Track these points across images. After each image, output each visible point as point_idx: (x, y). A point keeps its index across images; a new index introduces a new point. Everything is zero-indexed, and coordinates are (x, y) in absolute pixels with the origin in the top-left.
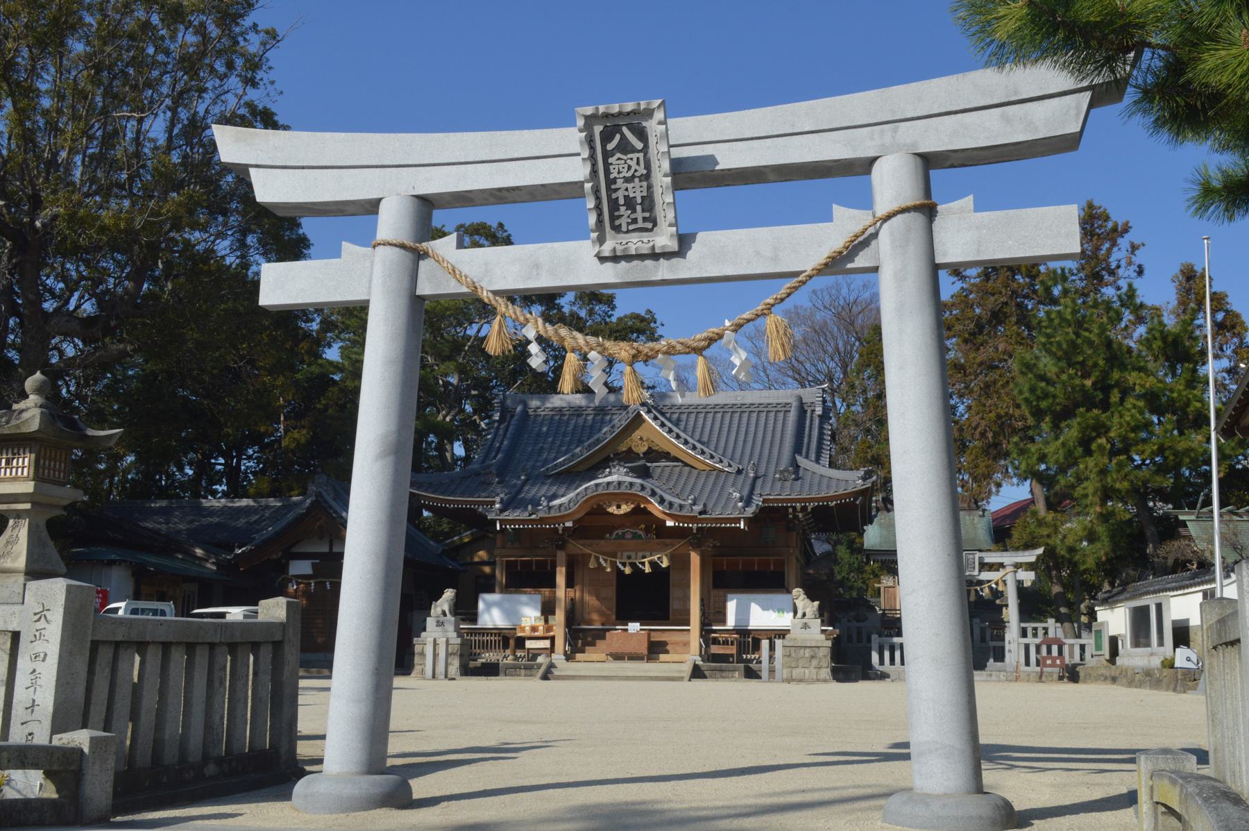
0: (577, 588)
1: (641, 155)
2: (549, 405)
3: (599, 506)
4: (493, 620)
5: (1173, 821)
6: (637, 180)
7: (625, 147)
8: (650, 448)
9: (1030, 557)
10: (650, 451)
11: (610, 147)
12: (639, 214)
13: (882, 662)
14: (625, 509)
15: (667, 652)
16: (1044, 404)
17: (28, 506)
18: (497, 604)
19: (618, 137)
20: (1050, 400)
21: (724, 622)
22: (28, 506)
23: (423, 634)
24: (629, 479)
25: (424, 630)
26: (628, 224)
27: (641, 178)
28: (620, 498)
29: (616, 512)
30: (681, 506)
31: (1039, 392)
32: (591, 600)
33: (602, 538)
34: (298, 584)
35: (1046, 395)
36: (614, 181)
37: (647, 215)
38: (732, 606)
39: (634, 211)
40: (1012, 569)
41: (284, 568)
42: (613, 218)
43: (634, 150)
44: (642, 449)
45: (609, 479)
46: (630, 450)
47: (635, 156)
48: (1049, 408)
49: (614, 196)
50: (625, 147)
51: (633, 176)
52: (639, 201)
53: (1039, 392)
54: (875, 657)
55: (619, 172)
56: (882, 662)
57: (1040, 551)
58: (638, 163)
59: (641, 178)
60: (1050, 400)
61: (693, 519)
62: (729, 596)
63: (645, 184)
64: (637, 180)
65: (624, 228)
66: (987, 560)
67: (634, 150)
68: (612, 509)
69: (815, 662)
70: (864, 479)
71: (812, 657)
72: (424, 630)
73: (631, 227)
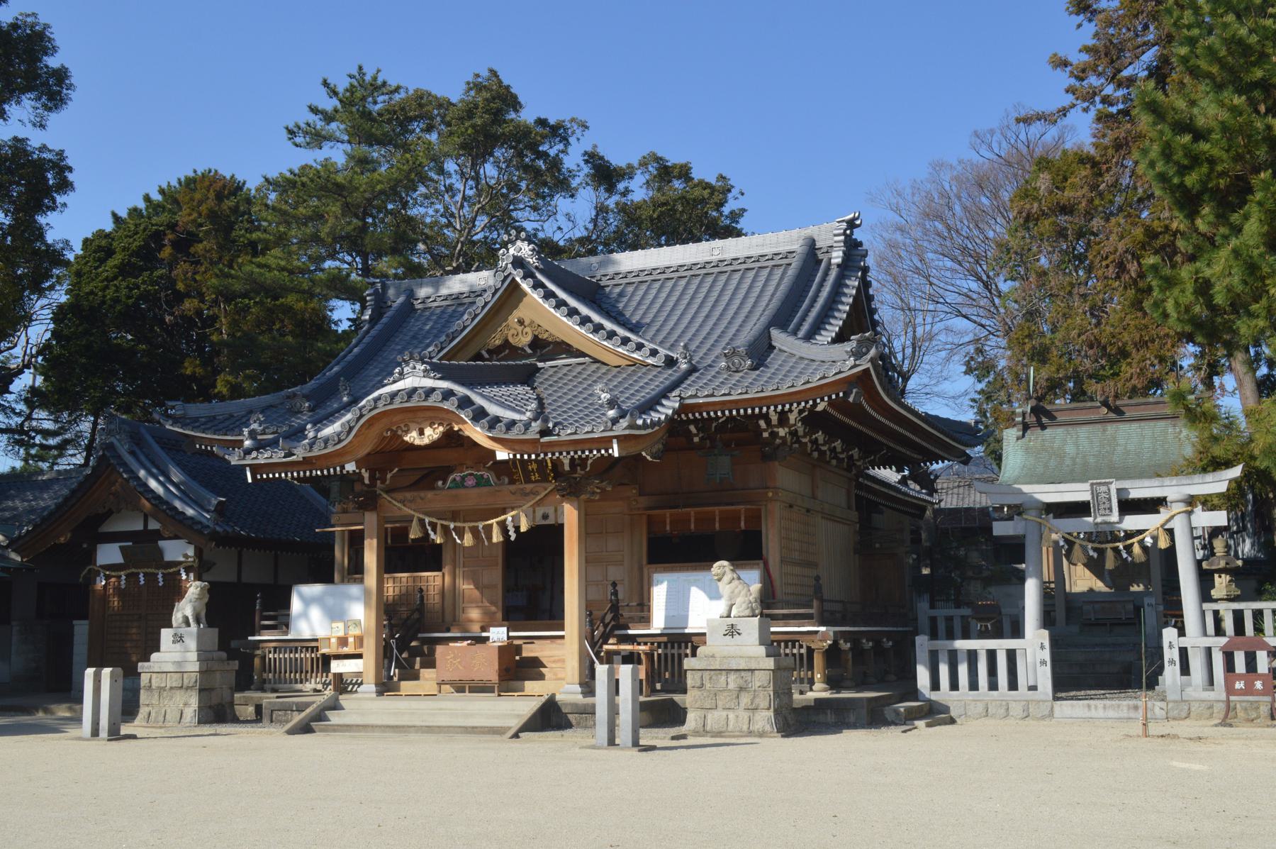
0: (446, 570)
2: (444, 291)
4: (312, 628)
8: (536, 338)
9: (1218, 483)
10: (537, 343)
13: (935, 686)
14: (432, 434)
15: (541, 677)
16: (1191, 180)
18: (317, 600)
20: (1205, 169)
21: (646, 620)
23: (154, 656)
24: (429, 383)
25: (158, 649)
28: (421, 415)
29: (417, 442)
30: (513, 423)
31: (1179, 156)
32: (466, 587)
34: (107, 578)
35: (1195, 160)
38: (659, 594)
40: (1181, 507)
41: (91, 556)
44: (524, 340)
45: (400, 385)
46: (506, 343)
48: (1204, 189)
53: (1179, 156)
54: (923, 676)
56: (935, 686)
57: (1236, 472)
60: (1205, 169)
62: (656, 576)
66: (1135, 494)
68: (412, 437)
69: (745, 699)
70: (857, 354)
71: (741, 689)
72: (158, 649)
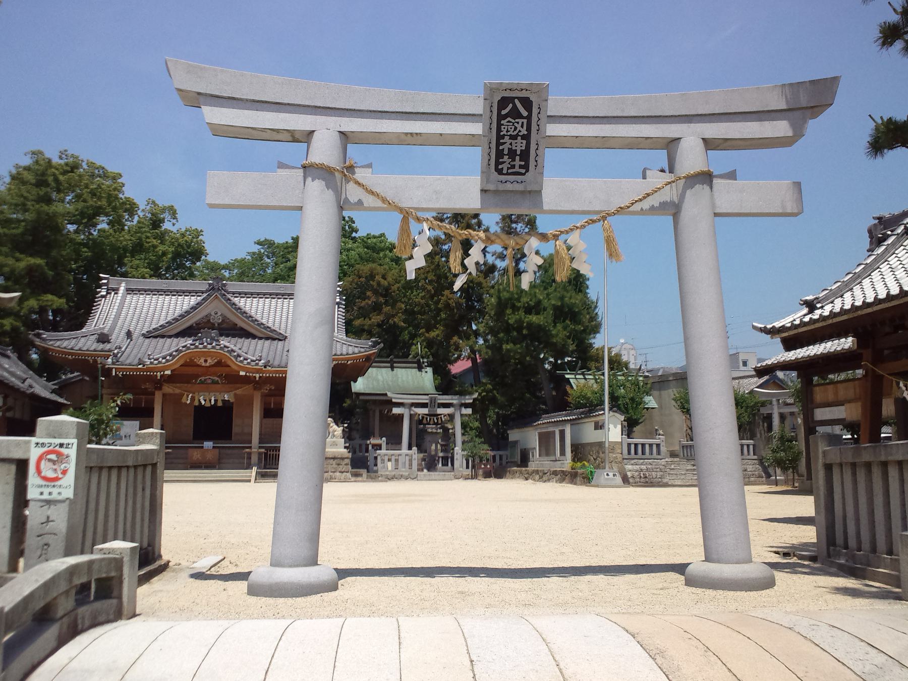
1: (525, 121)
3: (192, 360)
5: (203, 564)
6: (519, 138)
7: (515, 114)
11: (504, 112)
12: (518, 162)
14: (210, 362)
17: (847, 343)
19: (511, 105)
22: (847, 343)
26: (508, 168)
27: (523, 137)
29: (203, 364)
33: (188, 382)
36: (503, 137)
37: (523, 163)
39: (514, 160)
42: (497, 163)
43: (521, 117)
47: (520, 121)
49: (501, 148)
50: (515, 114)
51: (517, 135)
52: (518, 153)
55: (507, 131)
58: (522, 126)
59: (523, 137)
61: (258, 371)
63: (524, 142)
64: (519, 138)
65: (505, 171)
67: (521, 117)
73: (510, 171)
